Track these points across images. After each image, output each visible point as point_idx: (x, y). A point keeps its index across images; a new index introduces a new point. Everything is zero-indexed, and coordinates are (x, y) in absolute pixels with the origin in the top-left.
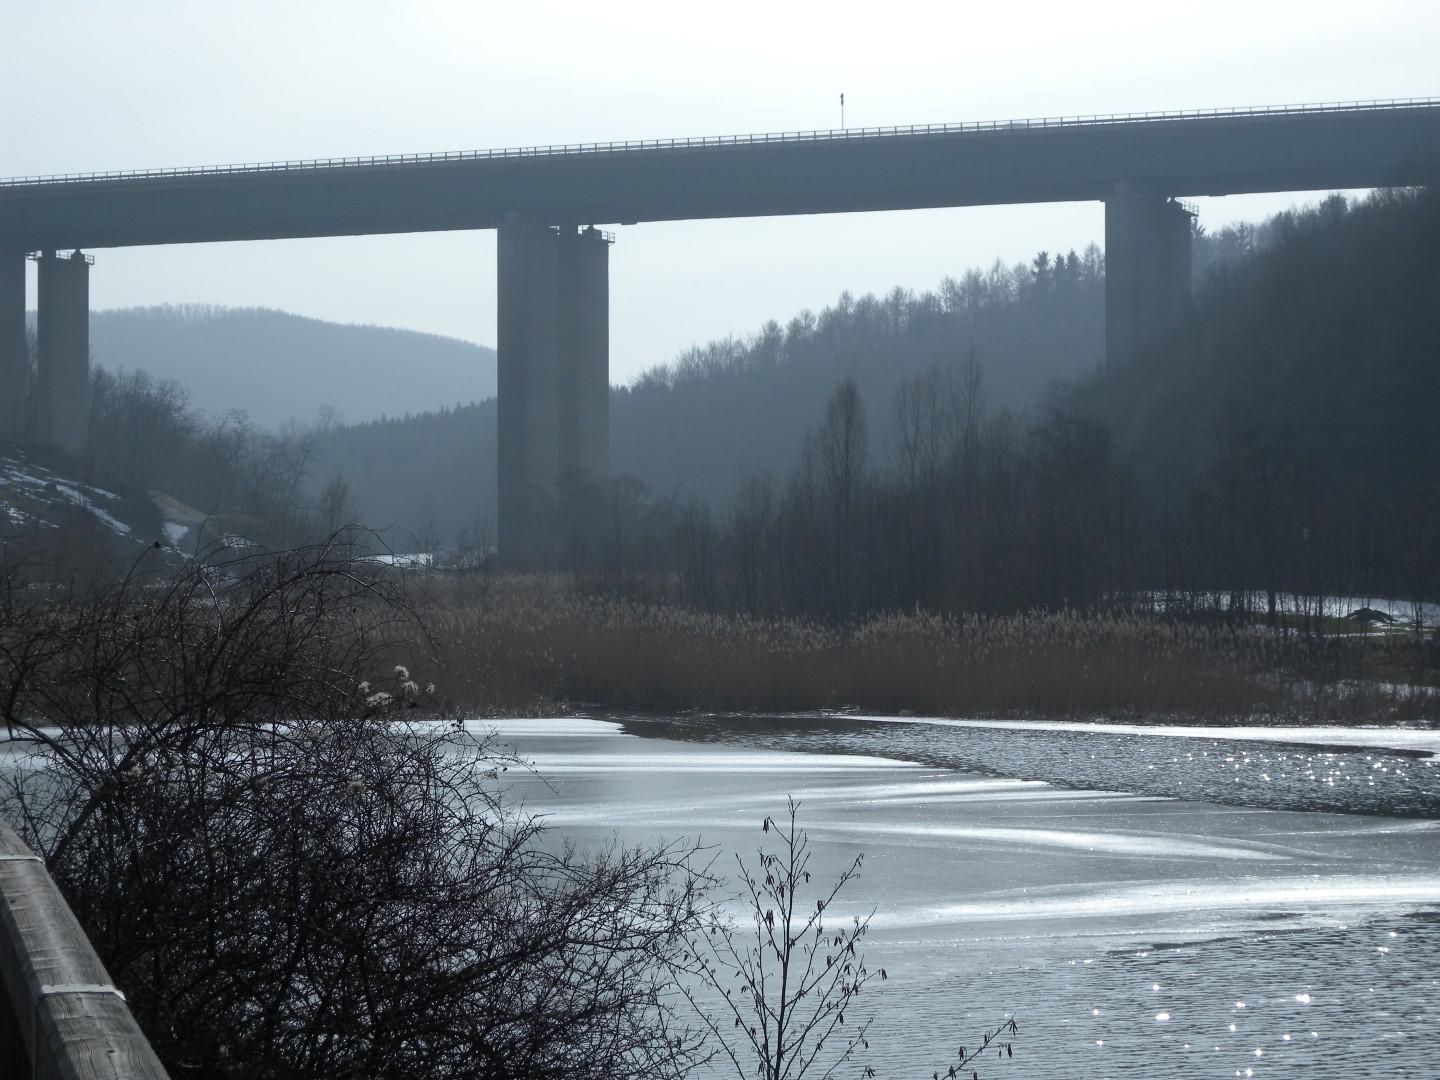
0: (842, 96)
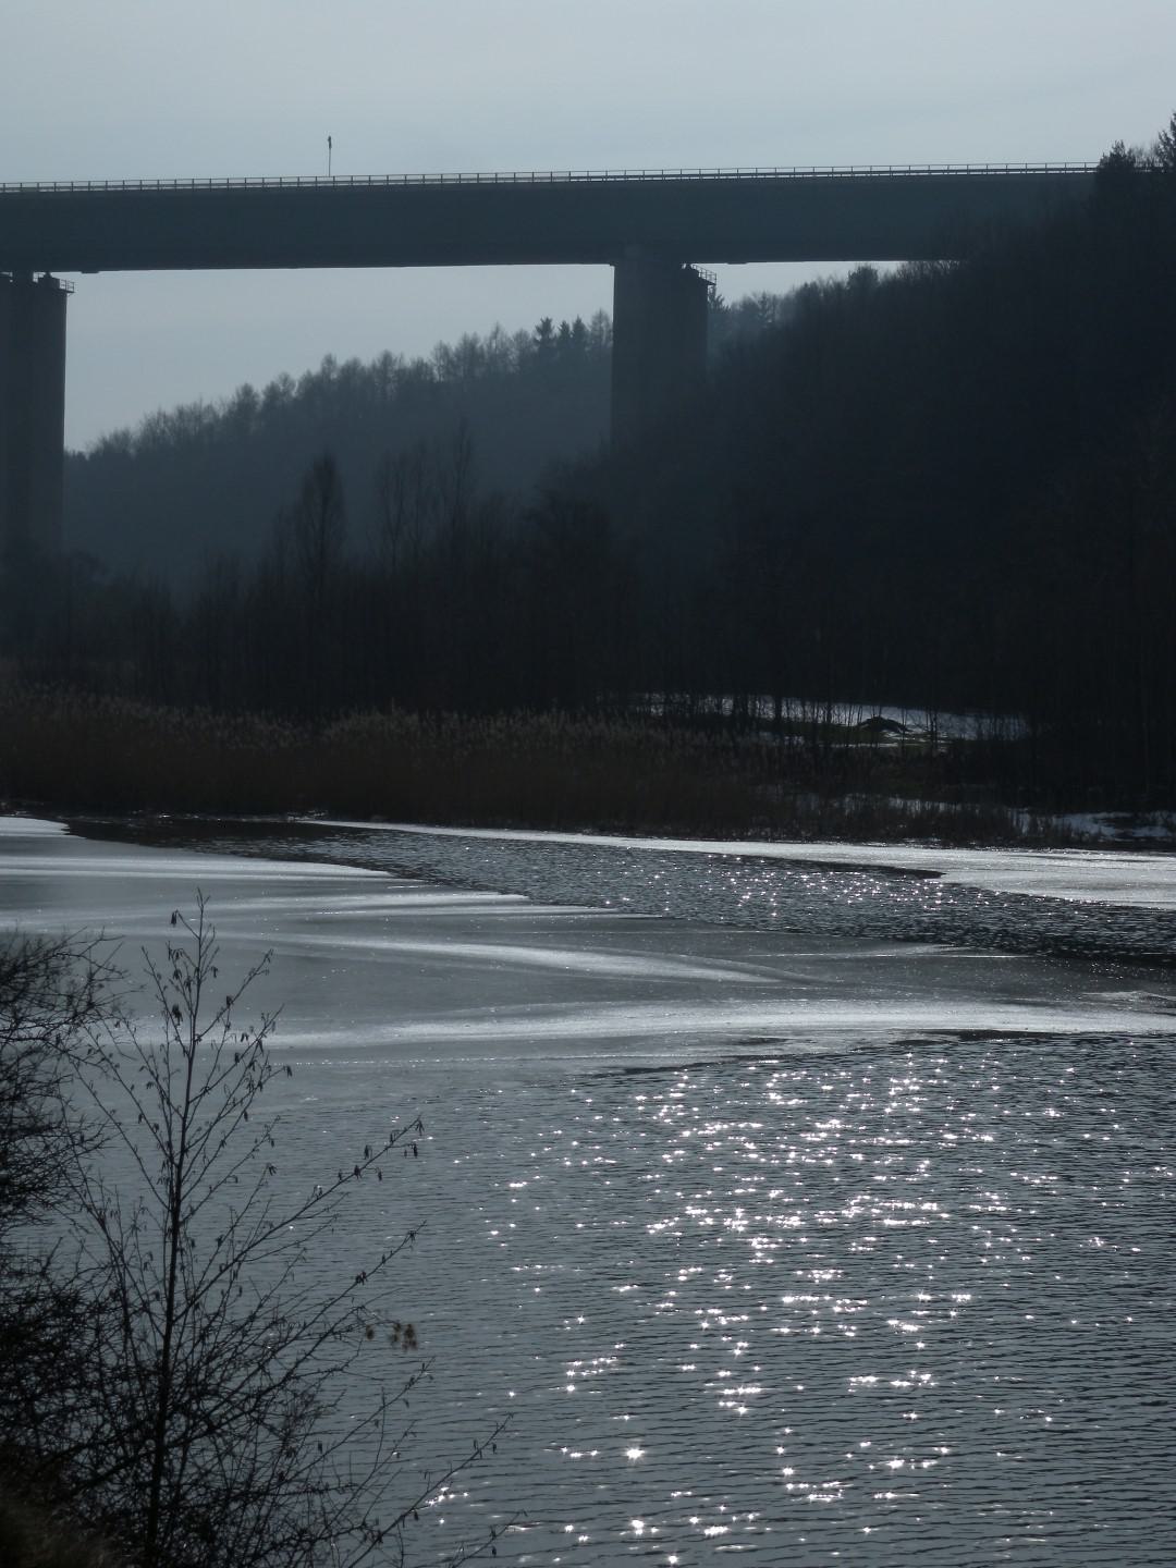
0: (330, 139)
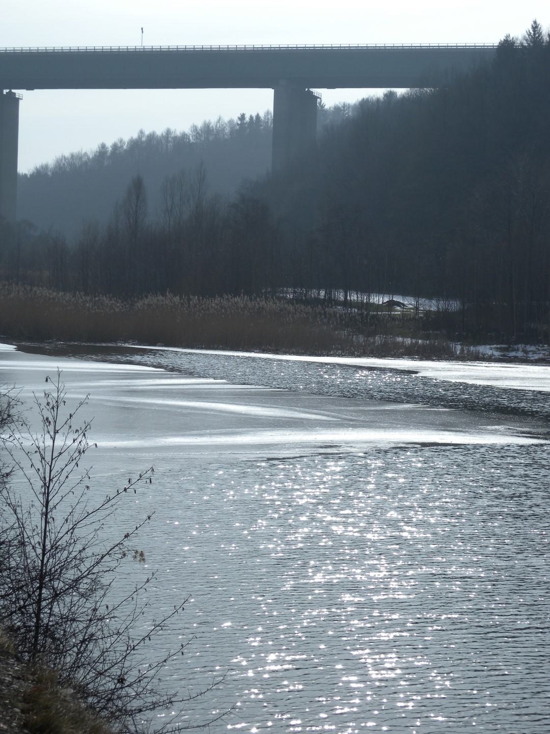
0: (142, 29)
